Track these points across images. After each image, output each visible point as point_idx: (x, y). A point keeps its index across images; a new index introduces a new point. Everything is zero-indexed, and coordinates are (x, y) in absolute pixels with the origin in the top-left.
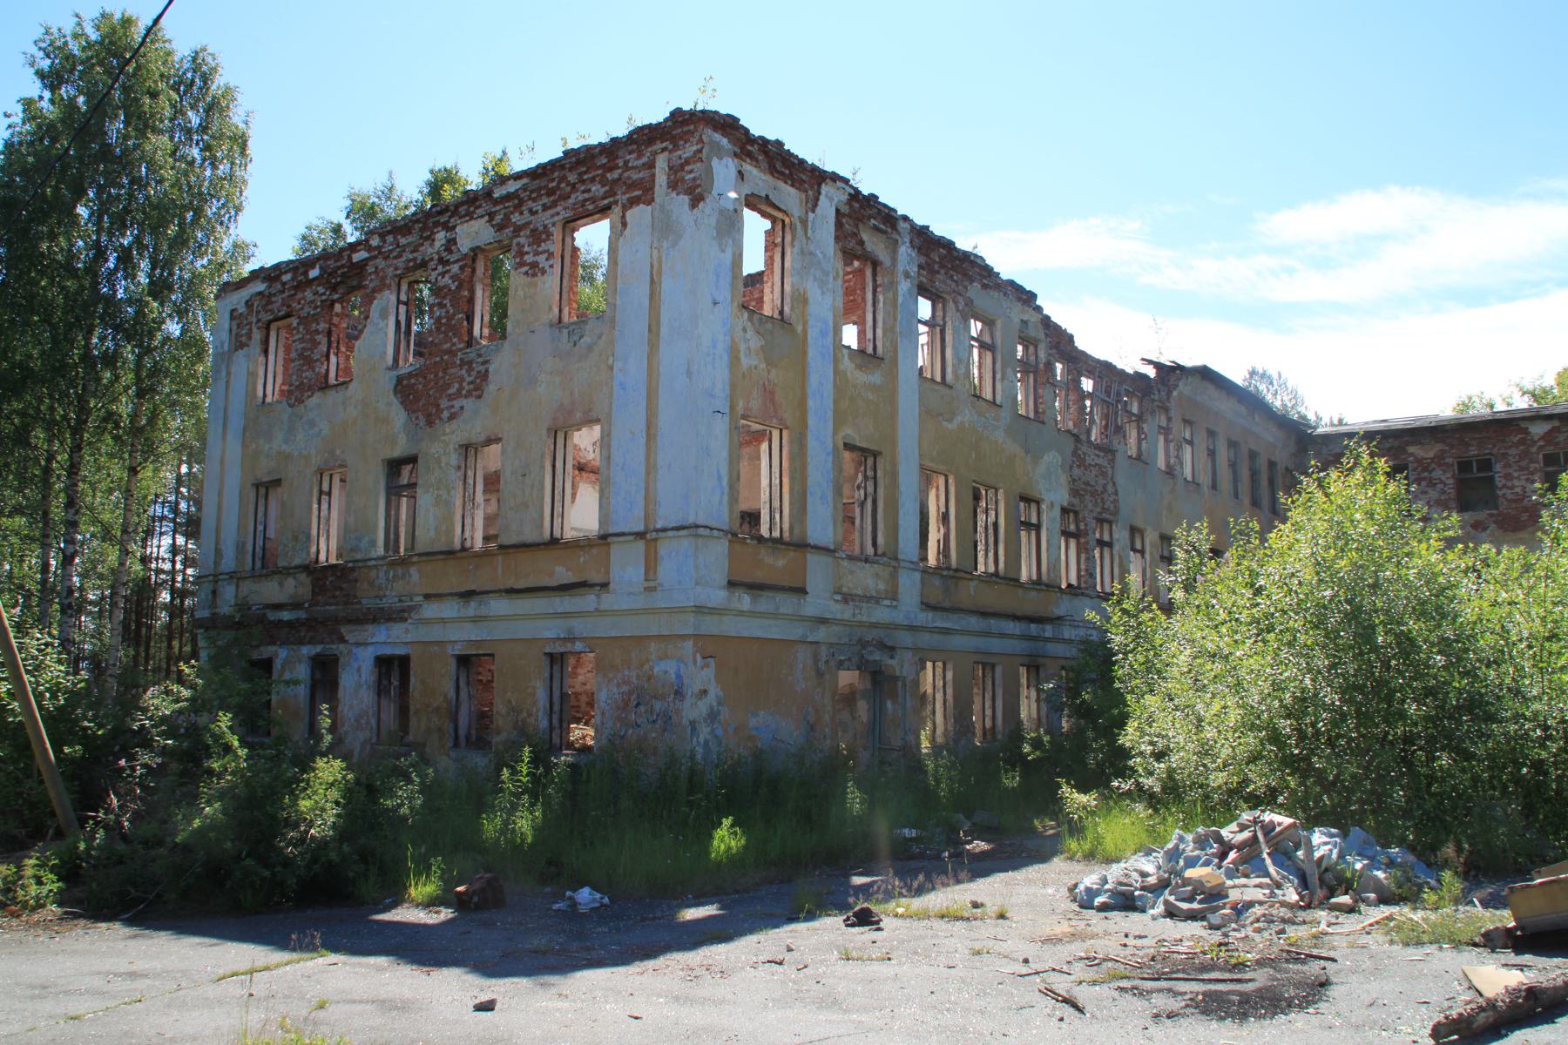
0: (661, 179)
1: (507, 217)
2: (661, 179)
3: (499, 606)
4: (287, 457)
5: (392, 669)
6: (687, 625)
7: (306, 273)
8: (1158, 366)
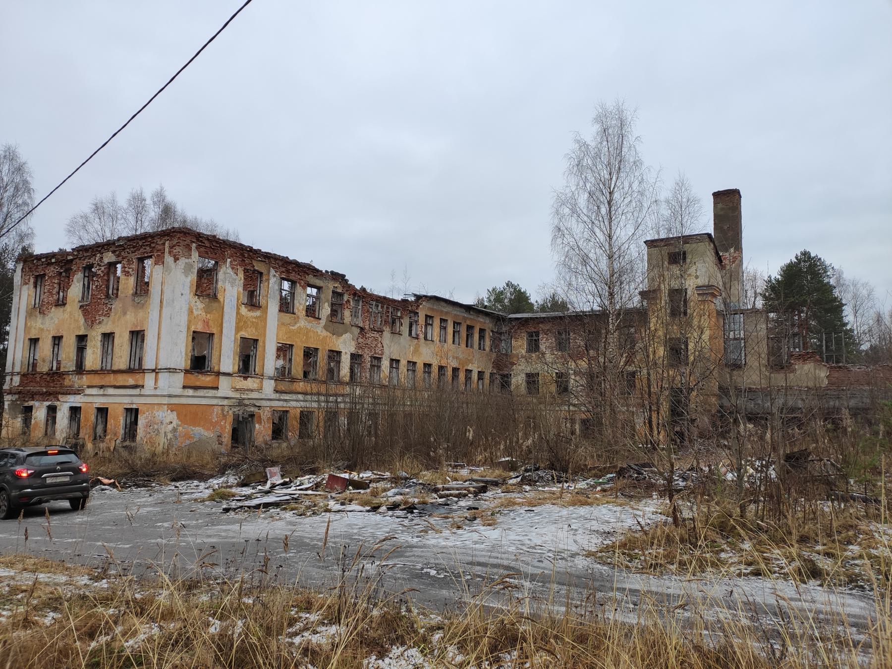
0: (167, 250)
1: (120, 253)
2: (167, 250)
3: (111, 391)
4: (42, 330)
5: (75, 411)
6: (165, 401)
7: (51, 259)
8: (415, 295)
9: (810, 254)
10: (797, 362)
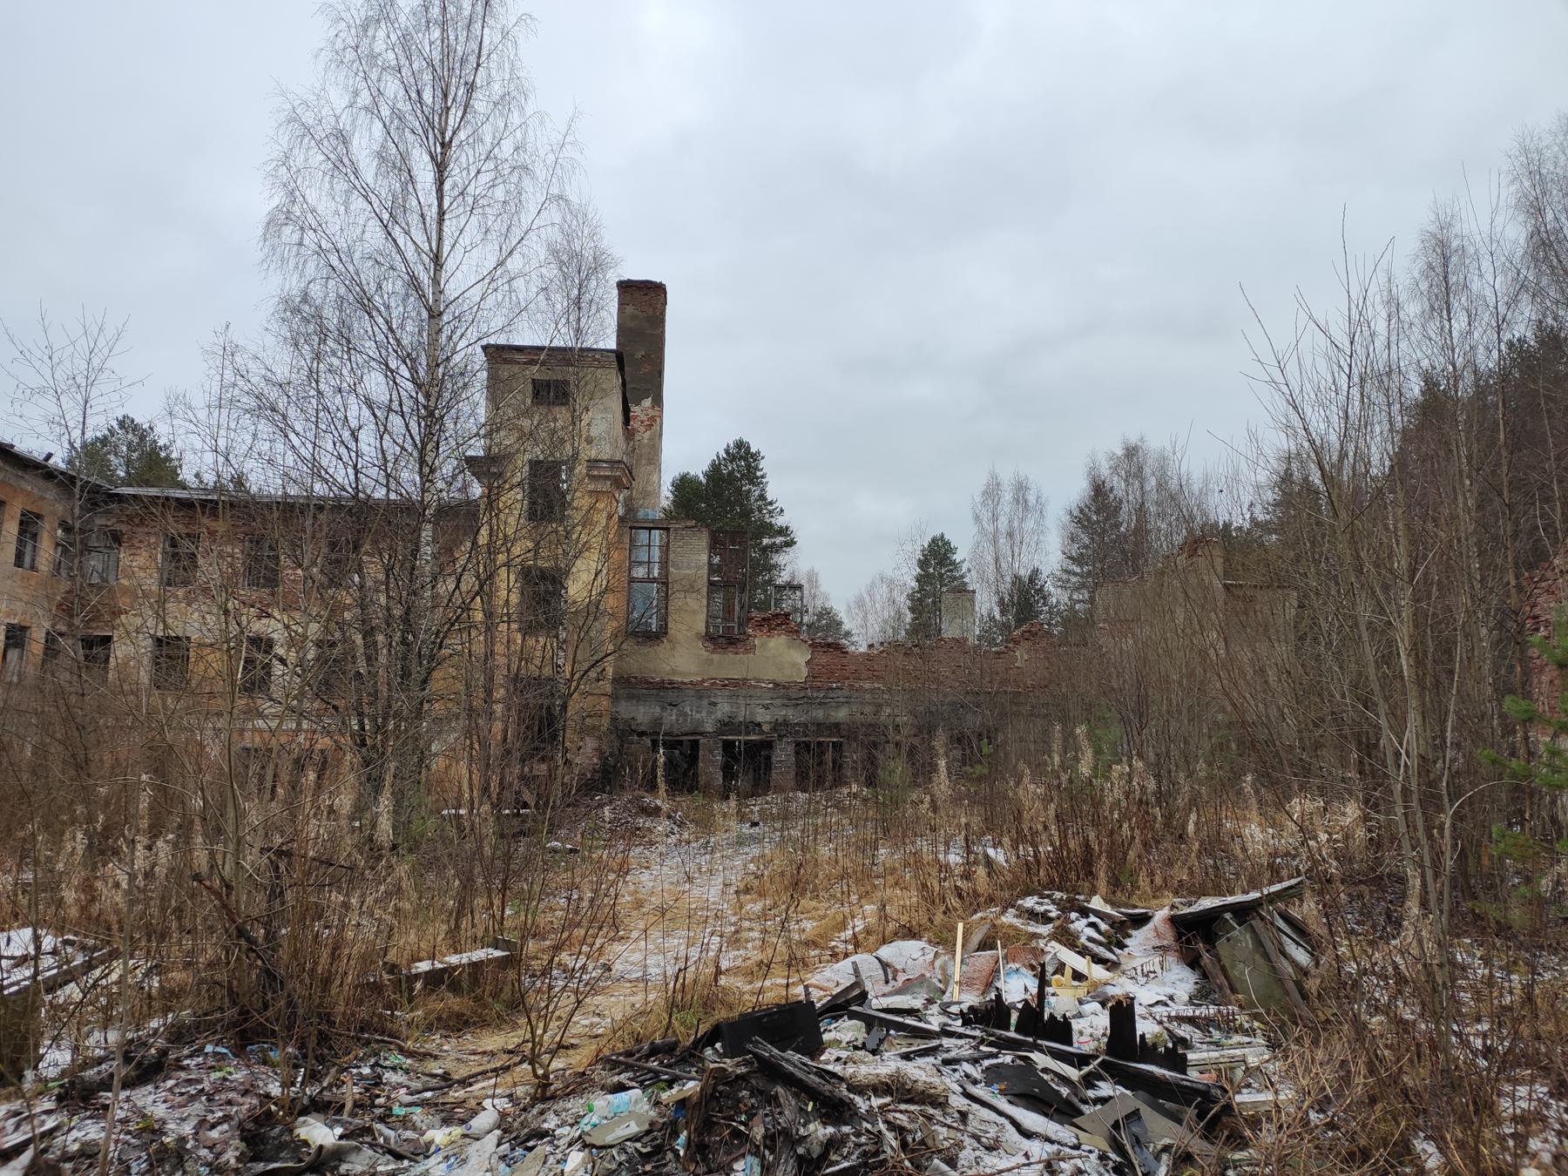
9: (749, 447)
10: (758, 633)
